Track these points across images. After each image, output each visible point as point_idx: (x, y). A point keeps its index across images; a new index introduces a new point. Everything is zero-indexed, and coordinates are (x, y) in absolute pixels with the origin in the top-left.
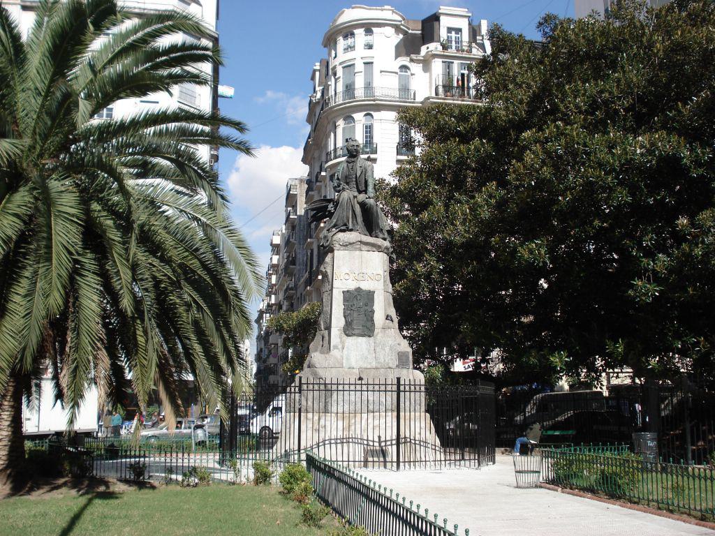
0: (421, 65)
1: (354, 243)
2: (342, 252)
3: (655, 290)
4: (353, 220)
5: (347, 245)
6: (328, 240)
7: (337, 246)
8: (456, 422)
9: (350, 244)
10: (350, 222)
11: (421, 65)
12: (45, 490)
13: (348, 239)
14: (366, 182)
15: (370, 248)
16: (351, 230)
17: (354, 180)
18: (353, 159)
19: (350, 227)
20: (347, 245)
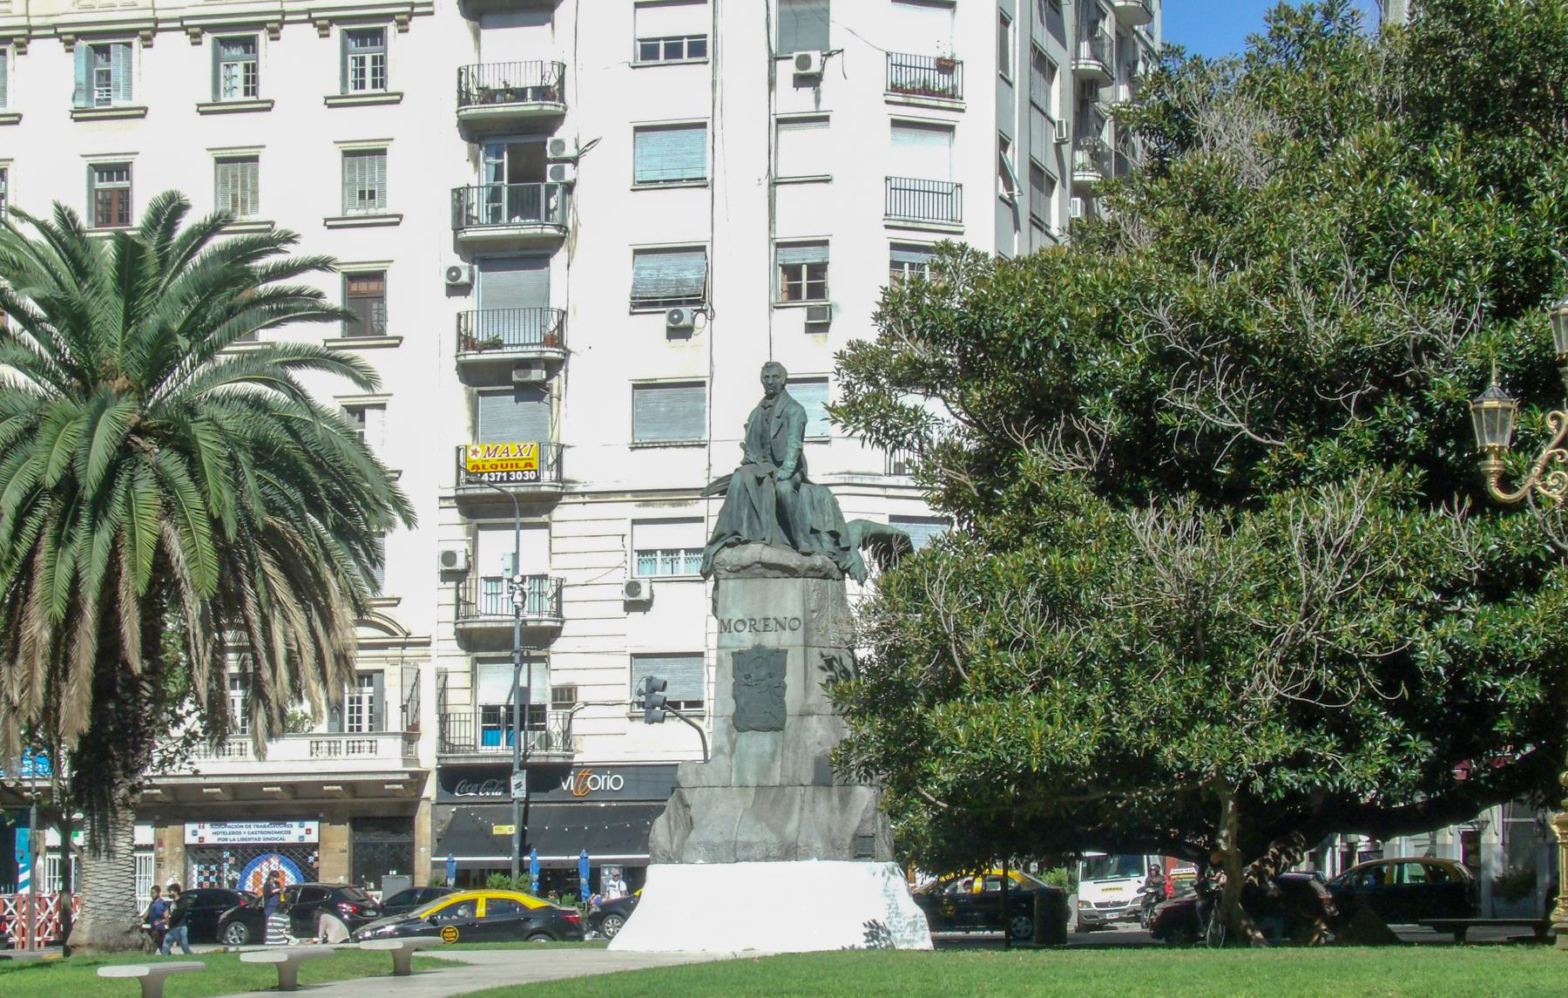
2: (731, 583)
9: (744, 568)
10: (745, 524)
15: (778, 573)
16: (747, 542)
19: (745, 536)
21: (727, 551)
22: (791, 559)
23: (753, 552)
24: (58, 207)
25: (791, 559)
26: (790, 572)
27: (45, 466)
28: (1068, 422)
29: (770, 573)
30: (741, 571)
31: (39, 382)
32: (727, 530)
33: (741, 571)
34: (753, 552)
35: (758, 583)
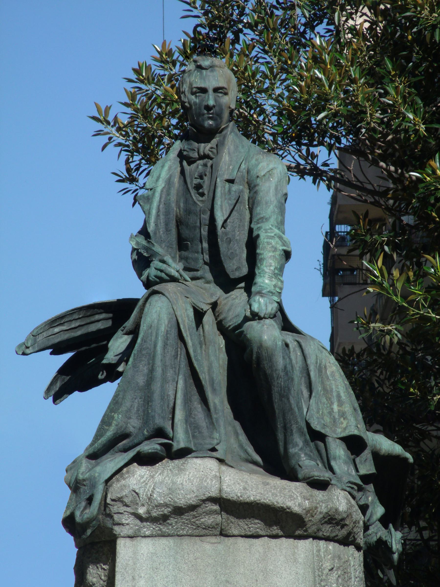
0: (312, 177)
1: (192, 508)
2: (146, 547)
3: (380, 17)
4: (189, 414)
5: (164, 518)
6: (90, 500)
7: (126, 523)
8: (407, 345)
9: (179, 511)
10: (179, 415)
11: (312, 177)
12: (173, 198)
13: (171, 491)
14: (252, 243)
15: (256, 525)
16: (184, 453)
17: (205, 232)
18: (205, 148)
19: (181, 440)
20: (164, 518)
21: (139, 475)
22: (290, 496)
23: (194, 478)
24: (95, 103)
25: (290, 496)
26: (284, 524)
27: (336, 463)
28: (414, 93)
29: (237, 526)
30: (171, 518)
31: (165, 345)
32: (134, 425)
33: (171, 518)
34: (194, 478)
35: (209, 547)
